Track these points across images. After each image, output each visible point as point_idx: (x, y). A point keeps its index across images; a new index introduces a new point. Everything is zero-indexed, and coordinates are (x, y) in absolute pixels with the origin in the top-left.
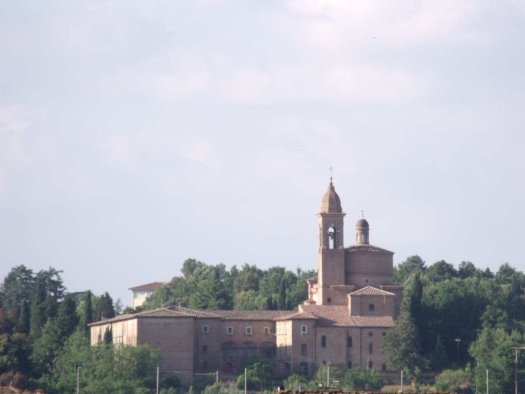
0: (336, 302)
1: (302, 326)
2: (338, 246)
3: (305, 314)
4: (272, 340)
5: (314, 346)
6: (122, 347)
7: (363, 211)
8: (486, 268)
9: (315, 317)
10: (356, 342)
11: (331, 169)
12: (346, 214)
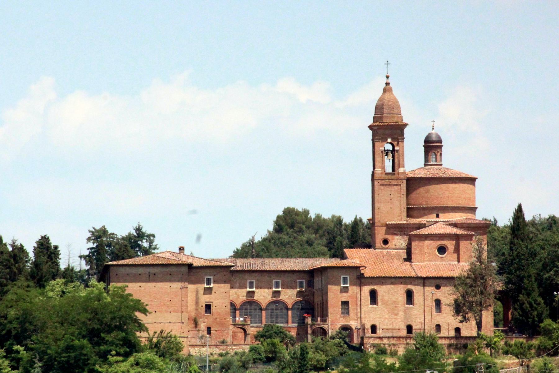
1: (248, 281)
2: (399, 167)
3: (248, 263)
4: (308, 298)
5: (359, 305)
6: (439, 364)
7: (433, 121)
10: (418, 297)
11: (387, 64)
12: (407, 125)
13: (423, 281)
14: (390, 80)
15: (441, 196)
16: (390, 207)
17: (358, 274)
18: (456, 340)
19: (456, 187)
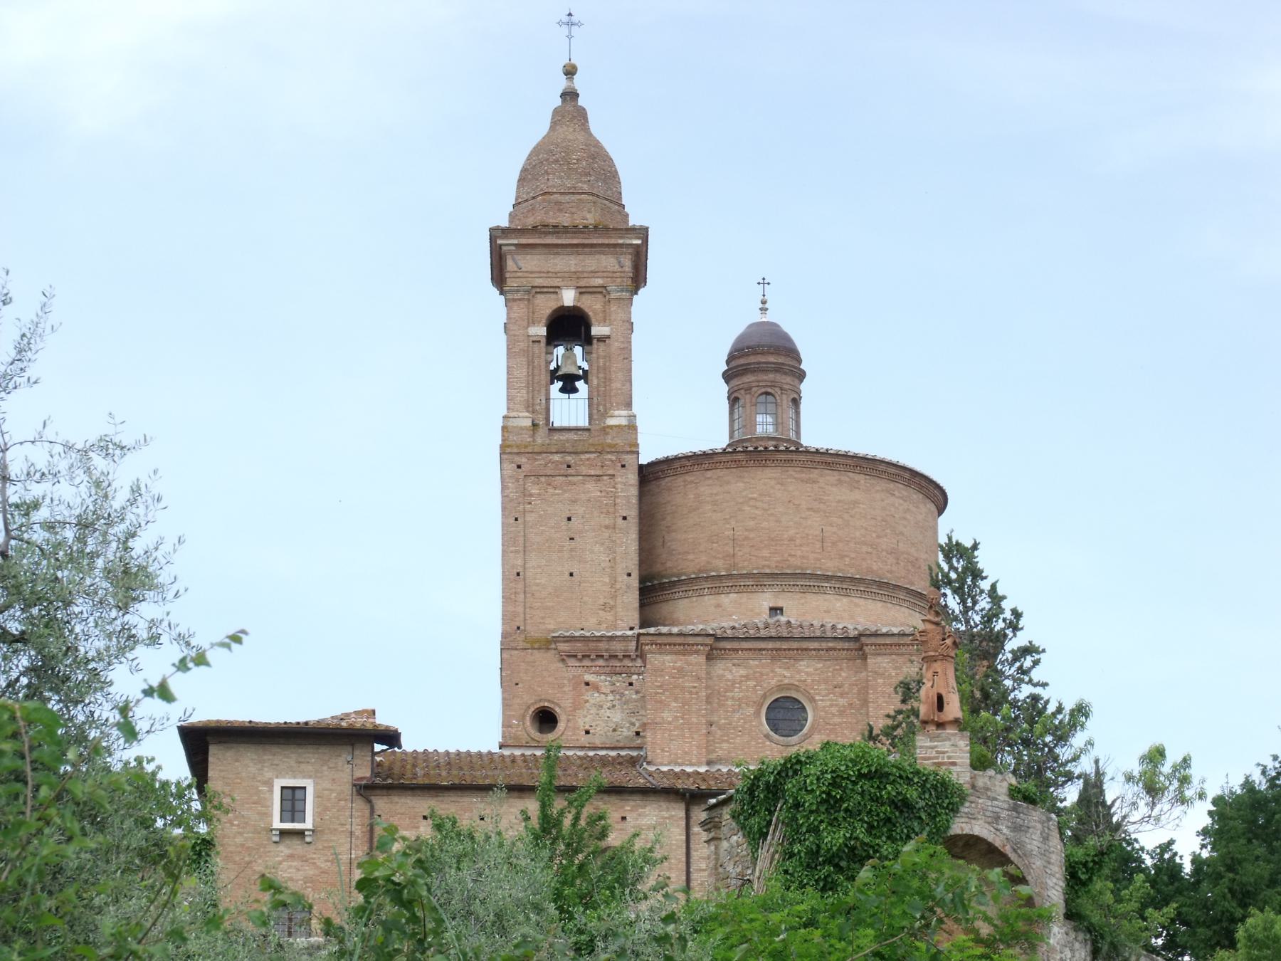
0: (587, 732)
1: (278, 784)
7: (764, 283)
8: (1242, 780)
9: (1265, 954)
13: (682, 814)
14: (579, 83)
15: (792, 532)
16: (568, 567)
17: (358, 774)
18: (574, 88)
19: (856, 503)
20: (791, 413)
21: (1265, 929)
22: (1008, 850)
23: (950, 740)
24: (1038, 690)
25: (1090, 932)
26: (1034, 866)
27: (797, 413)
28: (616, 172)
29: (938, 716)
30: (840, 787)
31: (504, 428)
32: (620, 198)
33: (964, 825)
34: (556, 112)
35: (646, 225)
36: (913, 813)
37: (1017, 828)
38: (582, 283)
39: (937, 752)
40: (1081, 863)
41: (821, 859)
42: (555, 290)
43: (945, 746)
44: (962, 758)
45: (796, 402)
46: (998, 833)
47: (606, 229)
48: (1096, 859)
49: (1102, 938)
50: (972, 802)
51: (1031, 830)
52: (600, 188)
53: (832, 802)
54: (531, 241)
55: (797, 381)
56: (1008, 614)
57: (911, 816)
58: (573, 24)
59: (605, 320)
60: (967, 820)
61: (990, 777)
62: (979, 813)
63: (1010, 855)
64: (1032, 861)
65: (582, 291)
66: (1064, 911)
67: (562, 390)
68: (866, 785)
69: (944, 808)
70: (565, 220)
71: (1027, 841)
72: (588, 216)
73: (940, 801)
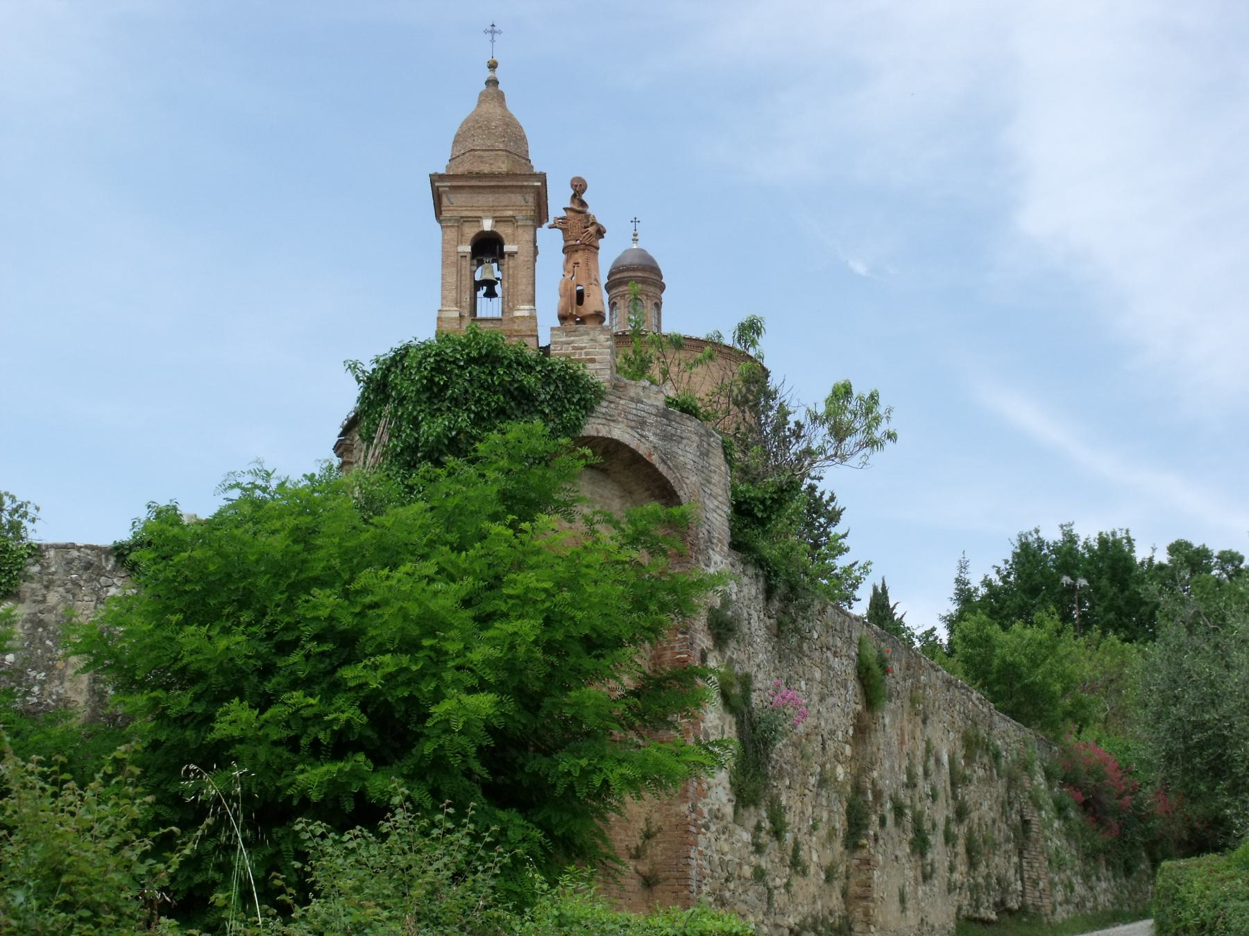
14: (499, 74)
20: (654, 312)
21: (978, 630)
22: (655, 459)
23: (588, 334)
24: (815, 482)
25: (762, 567)
26: (688, 481)
27: (659, 314)
28: (524, 136)
29: (577, 310)
30: (444, 372)
31: (439, 319)
32: (527, 155)
33: (600, 427)
34: (481, 94)
35: (544, 171)
36: (534, 405)
37: (667, 437)
38: (497, 214)
39: (574, 348)
40: (758, 499)
41: (419, 455)
42: (478, 220)
43: (583, 341)
44: (601, 354)
45: (658, 306)
46: (643, 440)
47: (516, 175)
48: (775, 496)
49: (776, 575)
50: (611, 402)
51: (685, 441)
52: (512, 146)
53: (435, 390)
54: (460, 184)
55: (658, 291)
56: (792, 425)
57: (532, 409)
58: (495, 32)
59: (513, 242)
60: (604, 421)
61: (644, 388)
62: (619, 415)
63: (657, 466)
64: (685, 475)
65: (498, 220)
66: (730, 540)
67: (486, 295)
68: (475, 369)
69: (573, 403)
70: (486, 169)
71: (680, 452)
72: (503, 166)
73: (568, 396)
